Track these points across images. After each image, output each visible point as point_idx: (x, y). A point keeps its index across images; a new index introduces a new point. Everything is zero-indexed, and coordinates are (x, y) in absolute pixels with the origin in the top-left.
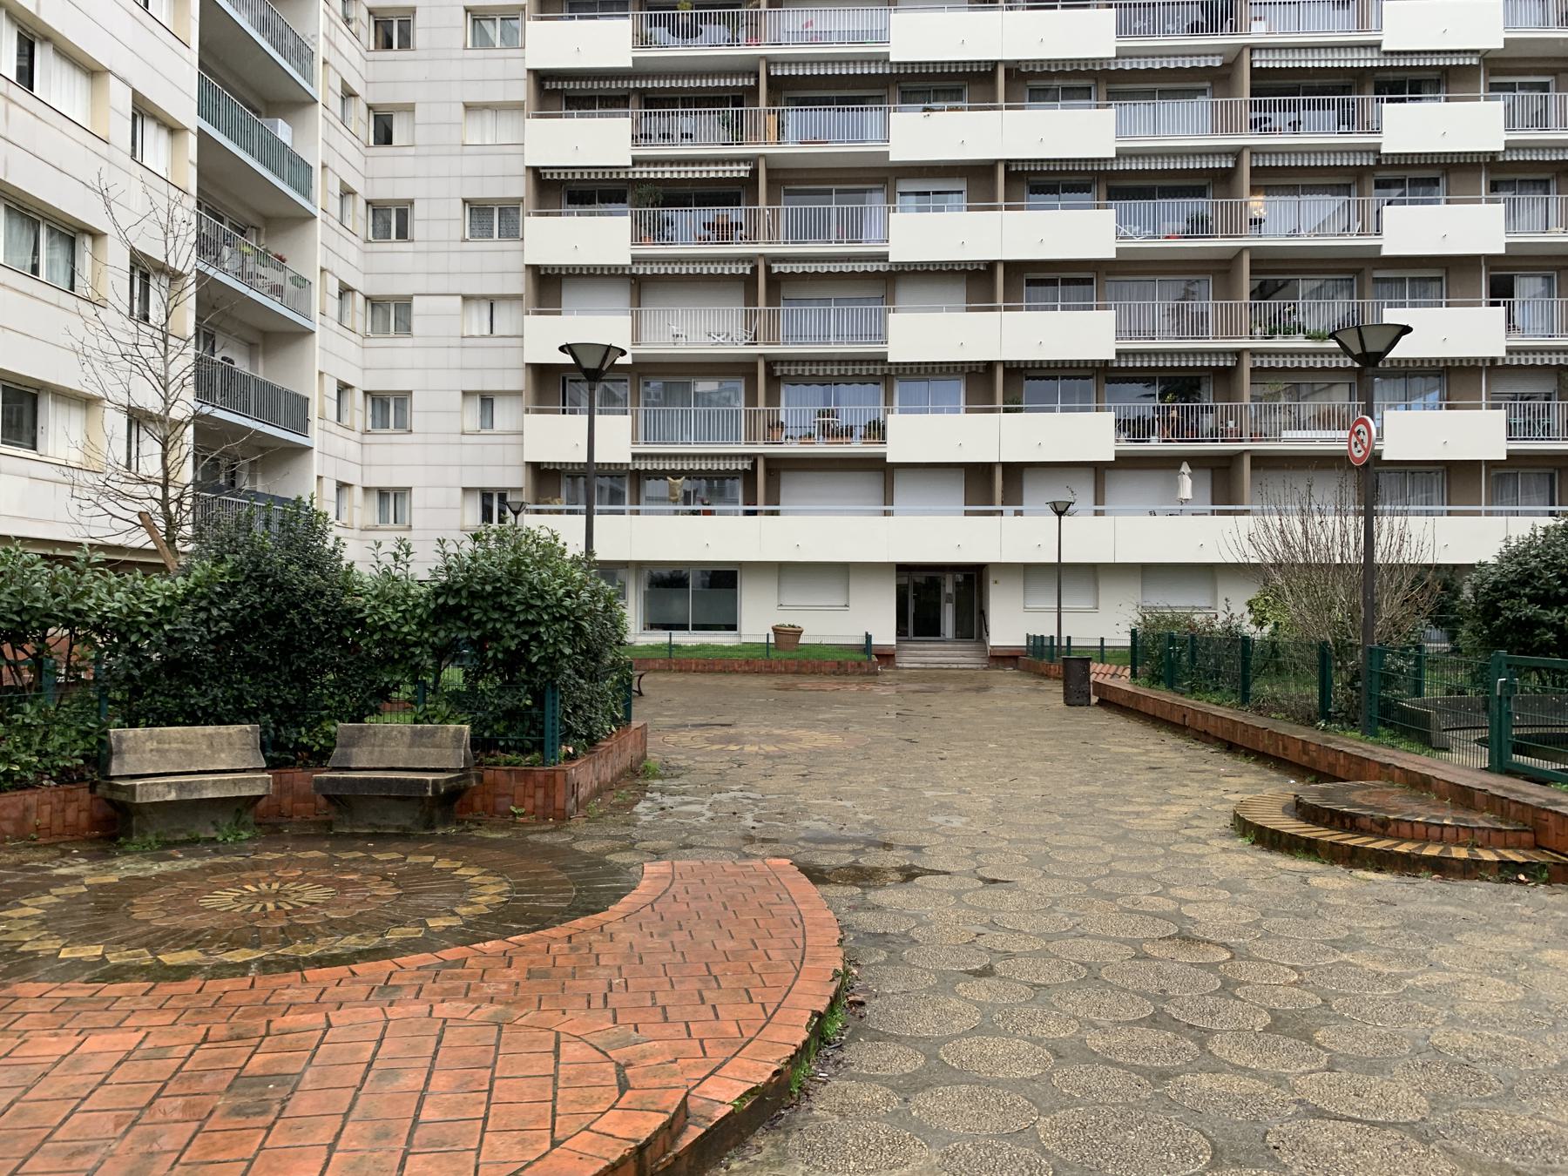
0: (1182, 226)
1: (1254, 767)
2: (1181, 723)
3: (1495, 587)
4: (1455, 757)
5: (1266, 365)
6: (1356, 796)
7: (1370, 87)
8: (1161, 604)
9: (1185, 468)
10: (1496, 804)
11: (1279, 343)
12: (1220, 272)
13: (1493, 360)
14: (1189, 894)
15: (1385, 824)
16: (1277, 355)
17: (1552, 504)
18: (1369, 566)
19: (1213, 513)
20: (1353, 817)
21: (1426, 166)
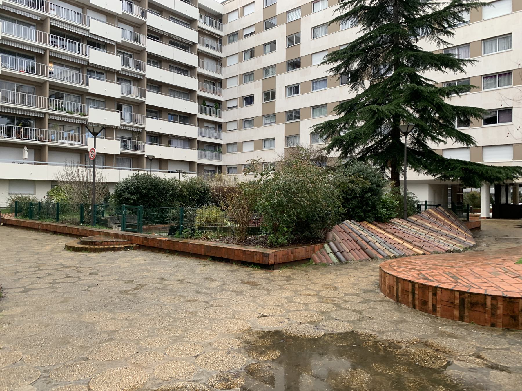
0: (25, 68)
1: (63, 237)
2: (38, 228)
3: (121, 190)
4: (113, 229)
5: (53, 119)
6: (94, 238)
7: (86, 42)
8: (18, 193)
9: (26, 148)
10: (123, 236)
11: (57, 112)
12: (39, 86)
13: (117, 127)
14: (62, 261)
15: (102, 243)
16: (57, 116)
17: (130, 167)
18: (94, 183)
19: (35, 164)
20: (95, 242)
21: (101, 69)
